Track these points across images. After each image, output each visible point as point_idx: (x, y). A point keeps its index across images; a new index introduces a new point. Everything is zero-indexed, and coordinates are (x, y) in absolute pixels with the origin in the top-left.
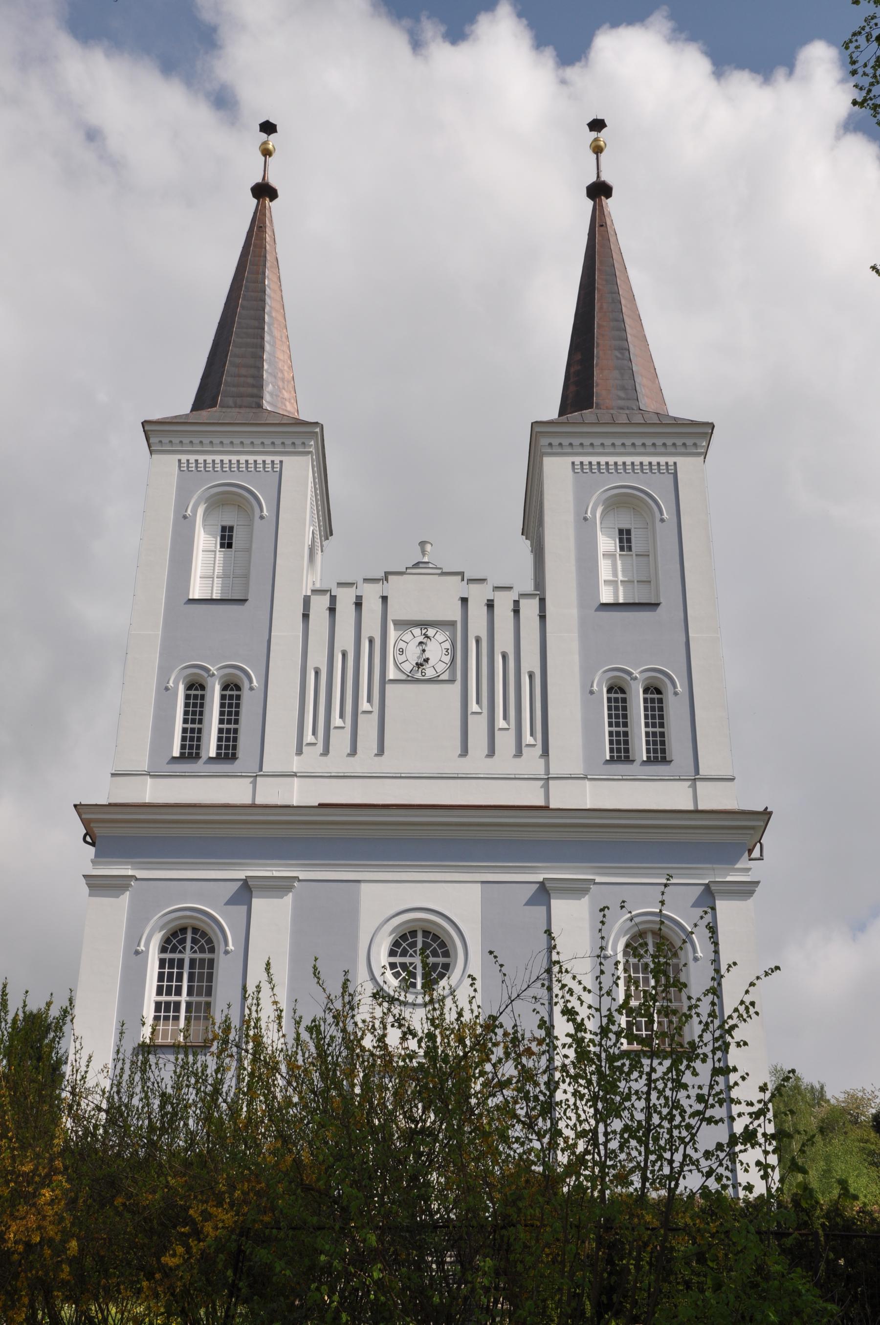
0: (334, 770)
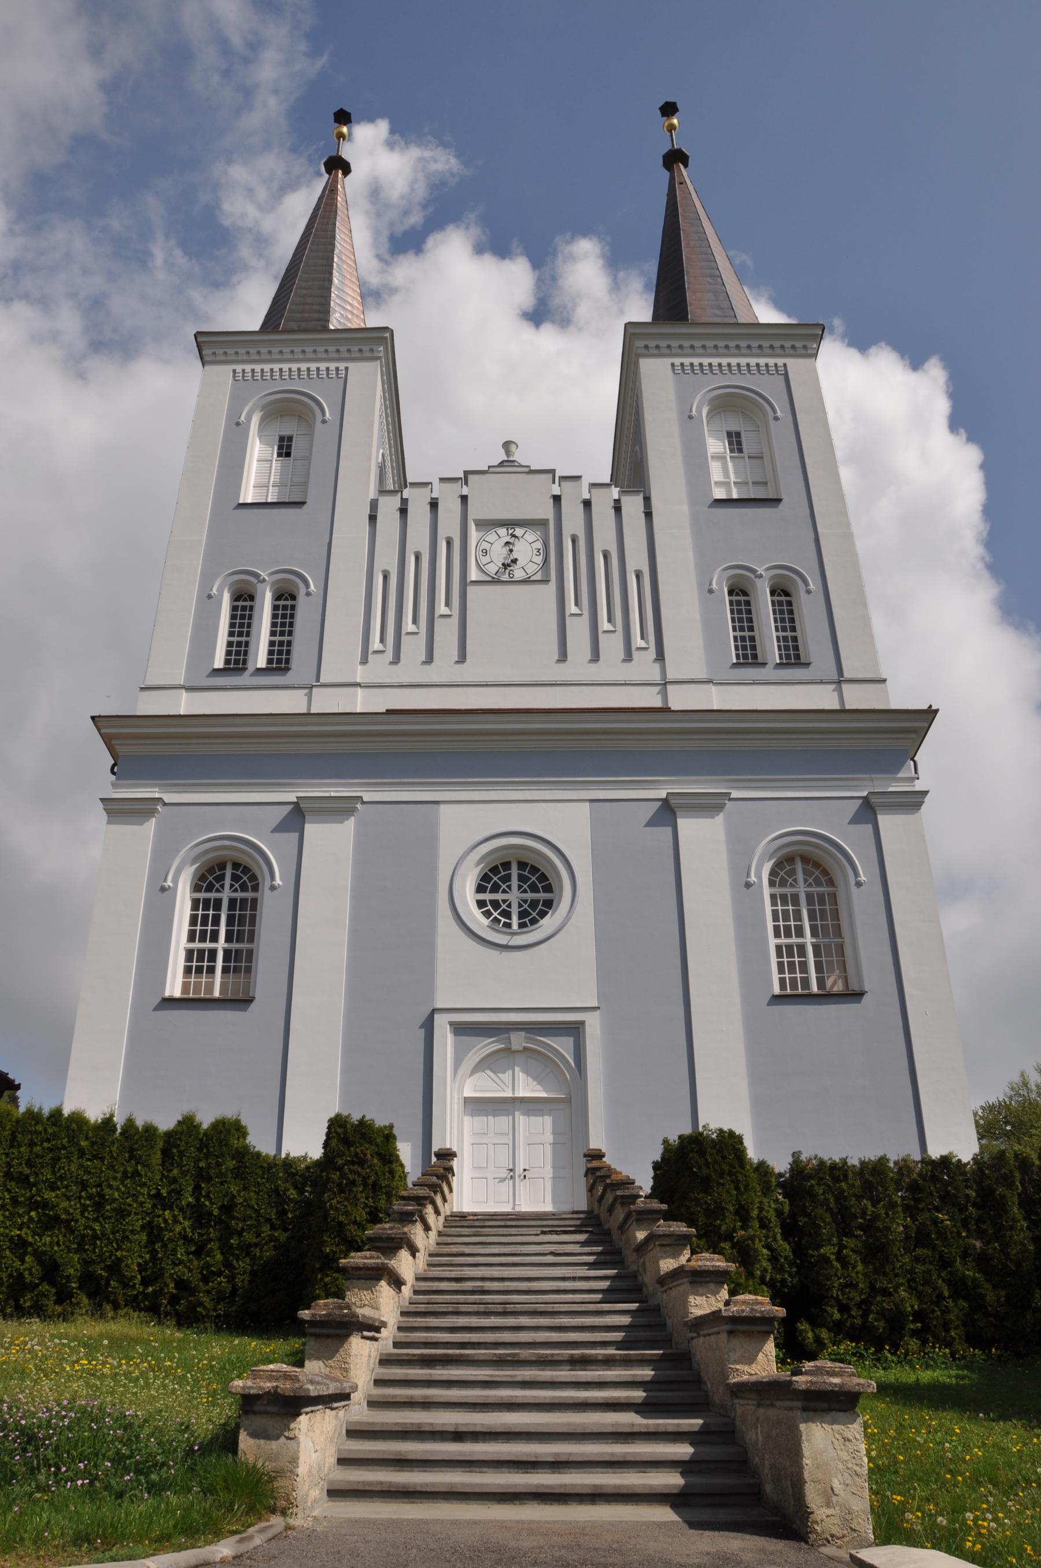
0: (406, 680)
